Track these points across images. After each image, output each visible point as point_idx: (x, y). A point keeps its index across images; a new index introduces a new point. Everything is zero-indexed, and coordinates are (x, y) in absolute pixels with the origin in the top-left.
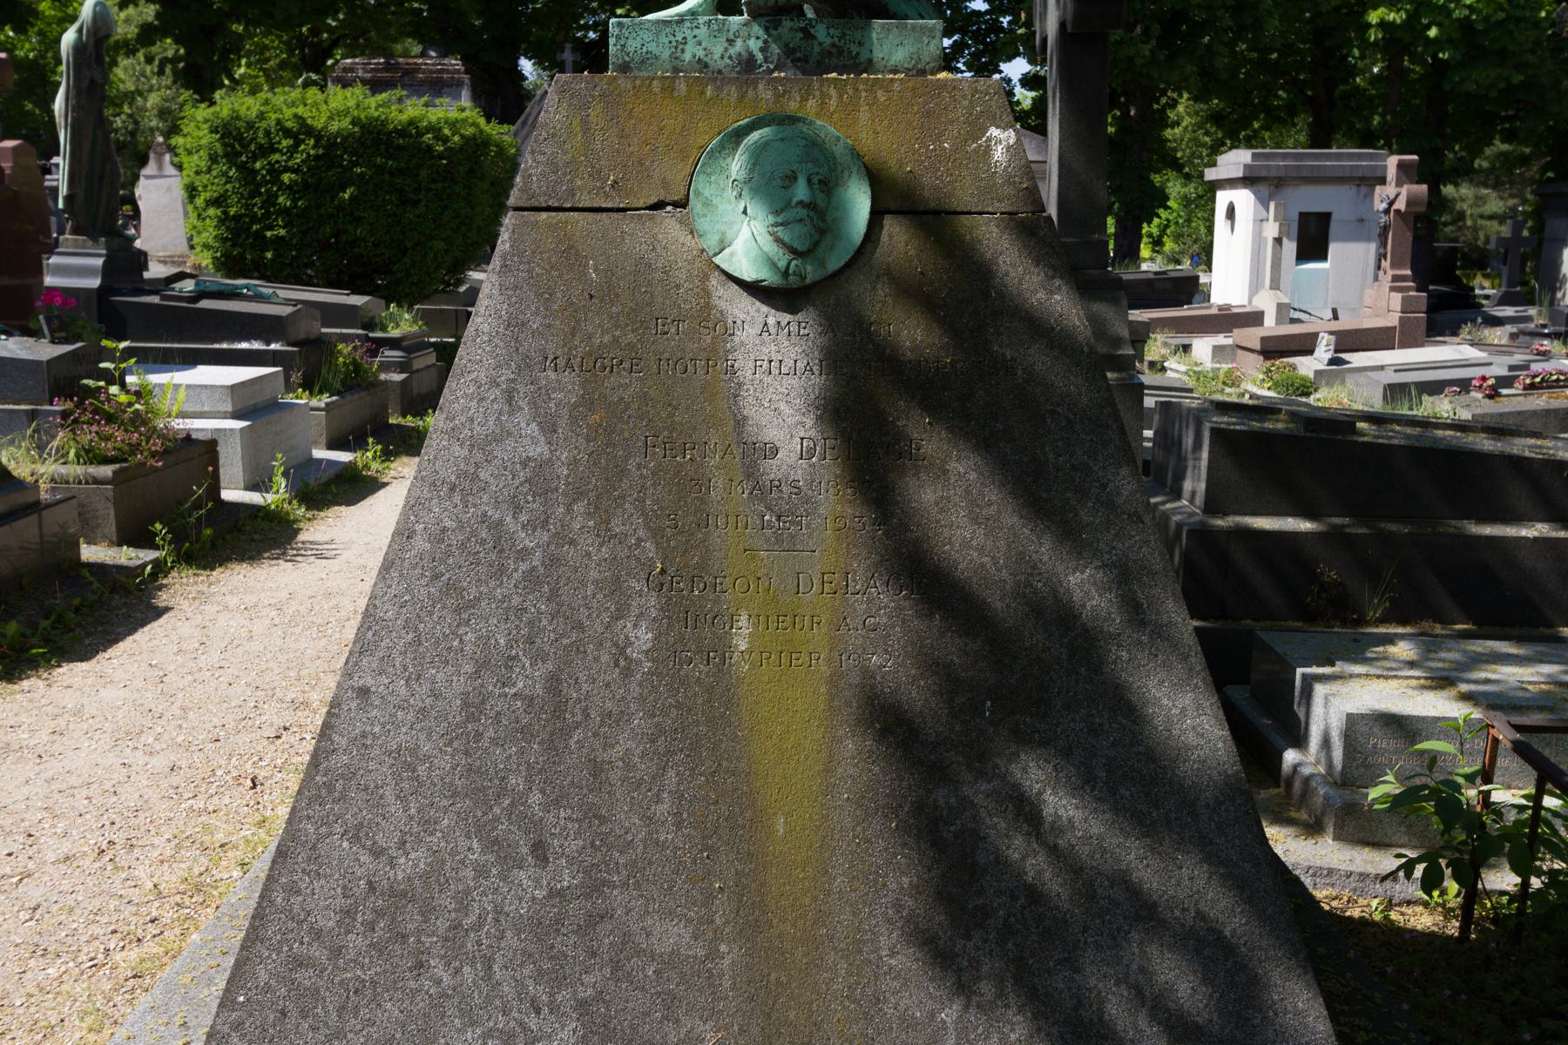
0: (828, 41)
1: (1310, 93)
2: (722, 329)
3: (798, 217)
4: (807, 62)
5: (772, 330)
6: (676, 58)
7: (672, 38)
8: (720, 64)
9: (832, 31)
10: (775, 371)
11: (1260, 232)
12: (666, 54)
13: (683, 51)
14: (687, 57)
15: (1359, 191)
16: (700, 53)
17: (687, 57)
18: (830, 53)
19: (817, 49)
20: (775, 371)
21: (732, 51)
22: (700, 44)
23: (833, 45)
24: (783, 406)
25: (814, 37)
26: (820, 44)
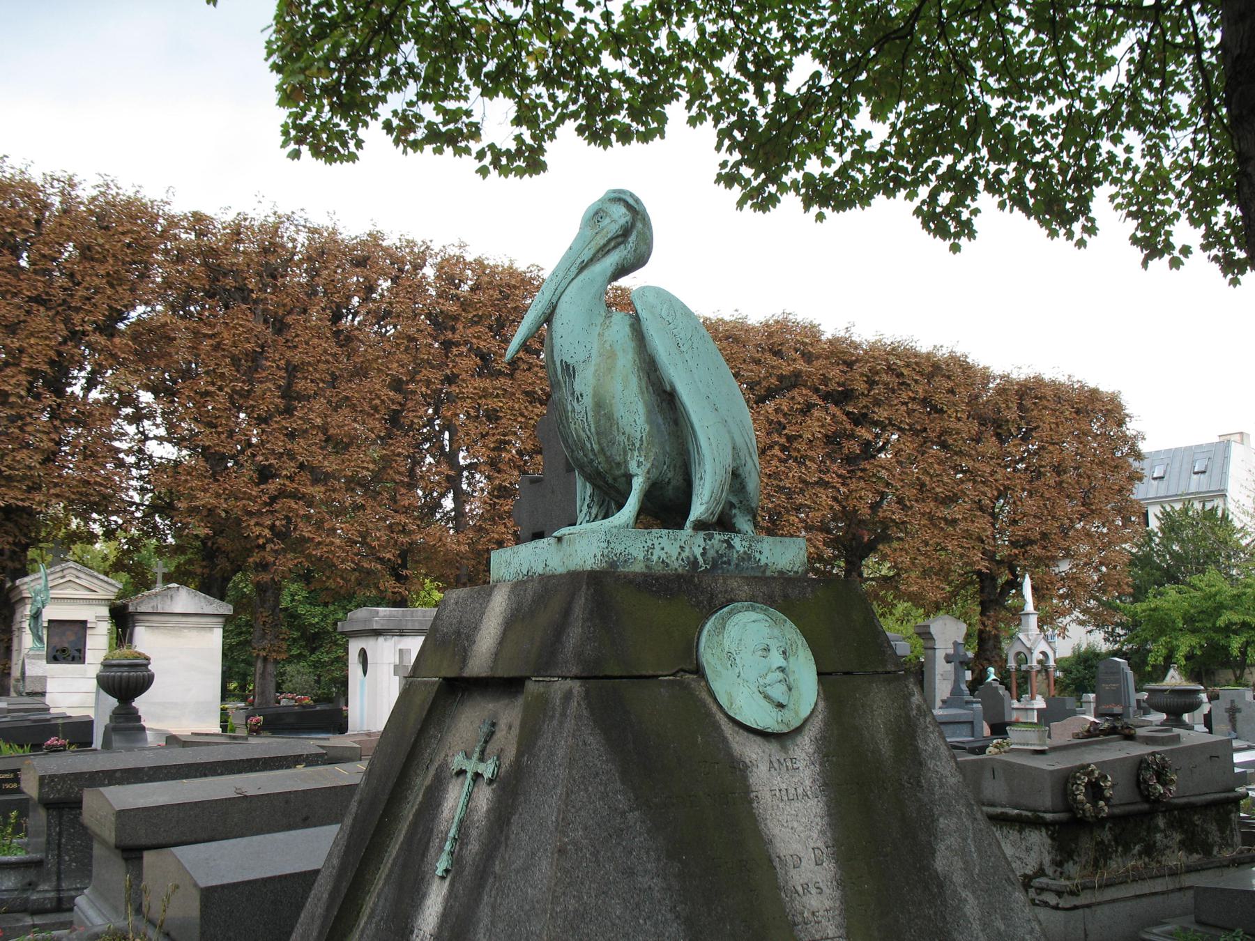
0: (742, 550)
1: (994, 54)
2: (739, 769)
3: (779, 679)
4: (730, 564)
5: (776, 765)
6: (648, 559)
7: (644, 544)
8: (676, 565)
9: (743, 543)
10: (785, 798)
11: (1051, 890)
12: (641, 557)
13: (652, 554)
14: (655, 558)
15: (61, 817)
16: (664, 556)
17: (655, 558)
18: (743, 558)
19: (735, 555)
20: (785, 798)
21: (684, 555)
22: (663, 549)
23: (745, 553)
24: (795, 824)
25: (733, 547)
26: (737, 552)
